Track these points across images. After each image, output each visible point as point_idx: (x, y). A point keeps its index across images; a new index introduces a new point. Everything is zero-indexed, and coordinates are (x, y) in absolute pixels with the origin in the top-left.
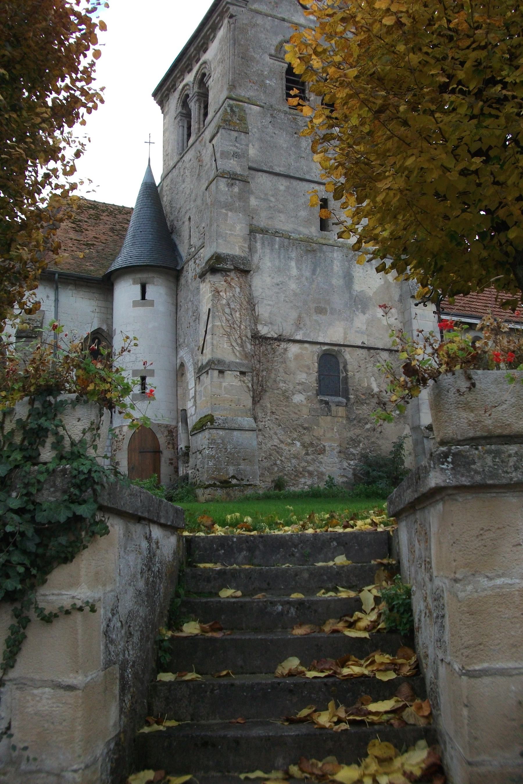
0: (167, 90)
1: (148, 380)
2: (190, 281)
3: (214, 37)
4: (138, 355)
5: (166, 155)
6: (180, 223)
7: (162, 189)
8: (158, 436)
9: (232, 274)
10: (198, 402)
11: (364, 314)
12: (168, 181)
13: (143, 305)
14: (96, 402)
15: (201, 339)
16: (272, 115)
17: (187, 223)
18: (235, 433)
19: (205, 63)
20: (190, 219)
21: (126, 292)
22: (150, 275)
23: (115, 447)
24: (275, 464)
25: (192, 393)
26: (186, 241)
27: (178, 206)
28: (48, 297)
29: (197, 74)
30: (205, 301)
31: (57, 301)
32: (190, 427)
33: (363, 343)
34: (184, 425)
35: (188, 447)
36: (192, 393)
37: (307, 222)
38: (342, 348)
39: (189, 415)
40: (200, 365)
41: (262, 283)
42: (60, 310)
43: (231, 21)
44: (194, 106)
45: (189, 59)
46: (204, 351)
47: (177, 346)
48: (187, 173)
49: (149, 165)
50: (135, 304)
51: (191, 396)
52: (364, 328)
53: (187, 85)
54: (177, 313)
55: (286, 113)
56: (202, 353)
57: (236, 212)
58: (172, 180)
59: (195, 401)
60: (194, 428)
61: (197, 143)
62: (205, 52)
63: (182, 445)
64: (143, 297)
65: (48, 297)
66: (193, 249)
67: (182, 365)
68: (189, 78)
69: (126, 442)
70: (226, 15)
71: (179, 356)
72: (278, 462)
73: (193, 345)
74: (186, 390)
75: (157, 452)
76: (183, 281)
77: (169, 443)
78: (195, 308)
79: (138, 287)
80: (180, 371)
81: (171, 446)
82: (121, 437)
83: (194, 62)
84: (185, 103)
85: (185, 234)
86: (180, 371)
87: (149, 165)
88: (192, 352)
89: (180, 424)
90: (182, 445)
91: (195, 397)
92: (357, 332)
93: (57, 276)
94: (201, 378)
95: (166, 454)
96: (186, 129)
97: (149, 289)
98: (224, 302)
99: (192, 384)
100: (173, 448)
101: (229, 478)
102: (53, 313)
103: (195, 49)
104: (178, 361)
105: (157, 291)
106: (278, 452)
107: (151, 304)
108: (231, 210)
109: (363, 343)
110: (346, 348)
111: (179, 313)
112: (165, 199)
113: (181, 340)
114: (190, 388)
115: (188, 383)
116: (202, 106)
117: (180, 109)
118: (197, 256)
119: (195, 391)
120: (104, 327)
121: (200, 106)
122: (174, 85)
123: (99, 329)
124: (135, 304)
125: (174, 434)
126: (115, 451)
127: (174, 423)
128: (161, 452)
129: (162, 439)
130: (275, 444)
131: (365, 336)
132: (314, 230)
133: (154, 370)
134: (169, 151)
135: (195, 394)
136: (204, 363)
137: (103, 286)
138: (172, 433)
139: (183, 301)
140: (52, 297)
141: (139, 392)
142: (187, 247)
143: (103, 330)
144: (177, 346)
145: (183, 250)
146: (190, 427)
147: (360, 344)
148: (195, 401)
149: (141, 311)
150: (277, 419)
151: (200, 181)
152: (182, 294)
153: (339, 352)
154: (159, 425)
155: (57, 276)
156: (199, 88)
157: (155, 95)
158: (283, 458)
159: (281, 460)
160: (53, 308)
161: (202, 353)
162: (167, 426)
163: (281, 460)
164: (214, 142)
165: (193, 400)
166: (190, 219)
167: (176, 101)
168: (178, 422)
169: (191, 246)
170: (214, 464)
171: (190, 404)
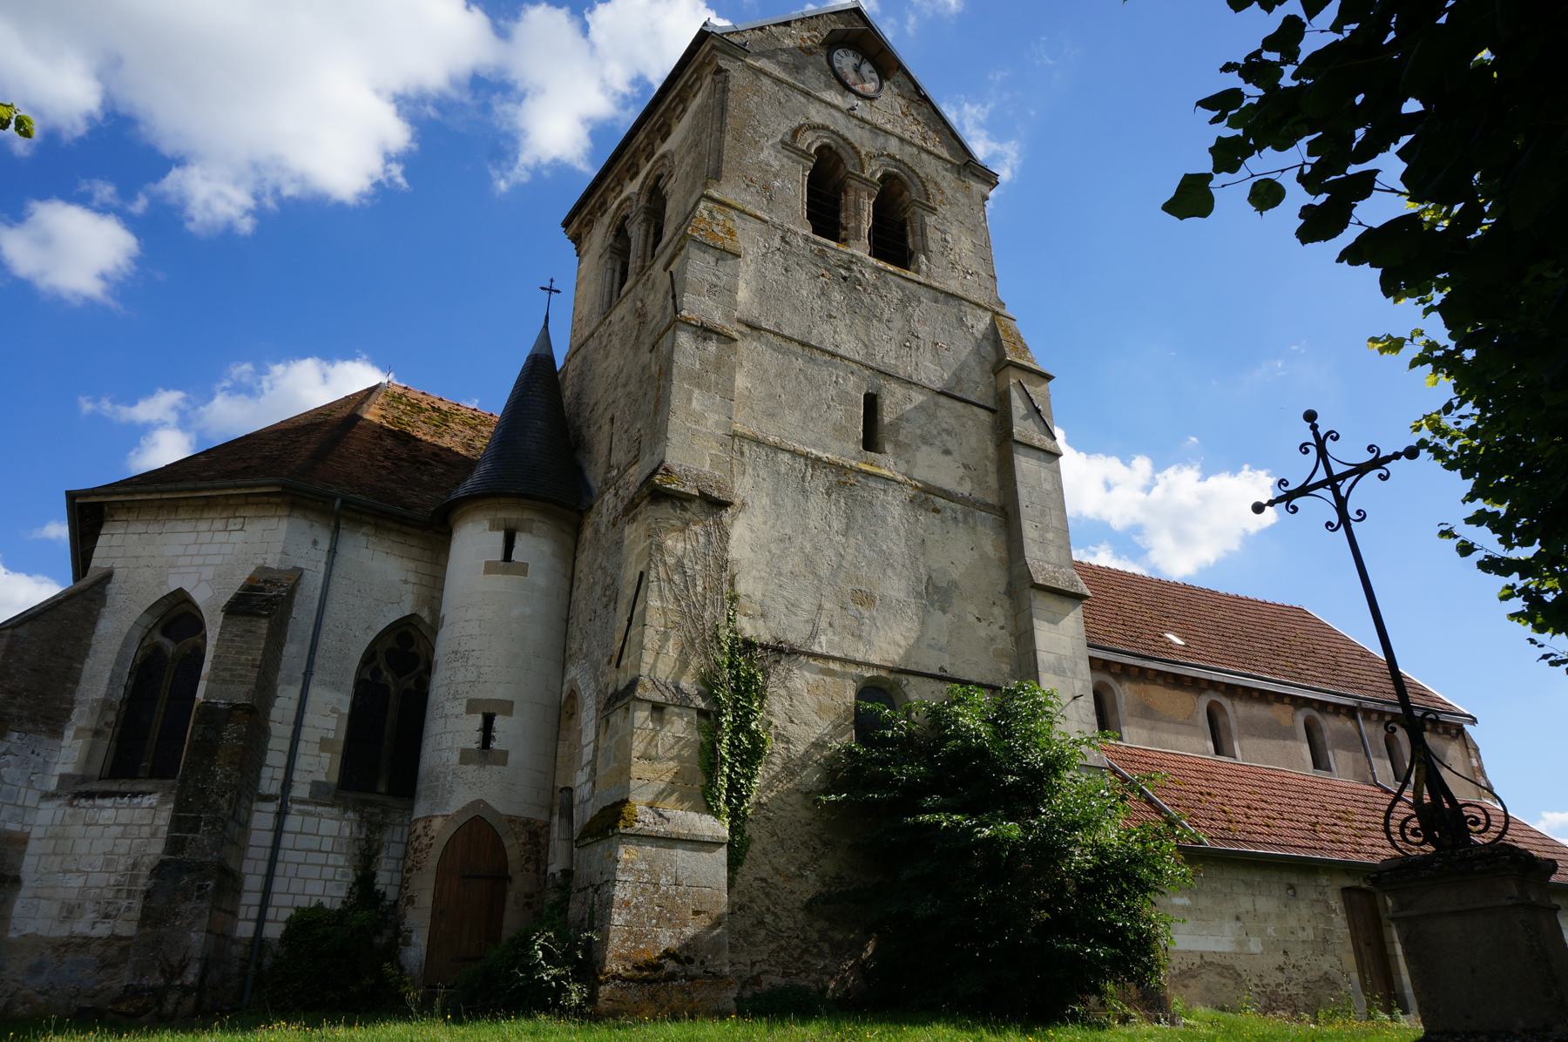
0: (590, 213)
1: (499, 722)
2: (603, 530)
3: (684, 110)
4: (484, 670)
5: (577, 321)
6: (594, 429)
7: (564, 376)
8: (507, 843)
9: (695, 507)
10: (601, 772)
11: (944, 611)
12: (577, 360)
13: (506, 572)
14: (1059, 778)
15: (619, 636)
16: (783, 238)
17: (606, 428)
18: (680, 854)
19: (664, 156)
20: (612, 419)
21: (475, 541)
22: (526, 515)
23: (410, 863)
24: (761, 923)
25: (587, 753)
26: (602, 460)
27: (592, 402)
28: (315, 543)
29: (646, 177)
30: (633, 558)
31: (333, 552)
32: (577, 827)
33: (941, 669)
34: (564, 821)
35: (567, 873)
36: (587, 753)
37: (840, 431)
38: (903, 677)
39: (576, 801)
40: (610, 691)
41: (745, 535)
42: (335, 570)
43: (718, 78)
44: (636, 232)
45: (633, 155)
46: (623, 663)
47: (563, 660)
48: (616, 341)
49: (546, 327)
50: (490, 568)
51: (584, 761)
52: (944, 640)
53: (628, 198)
54: (570, 593)
55: (807, 239)
56: (618, 666)
57: (709, 390)
58: (585, 358)
59: (594, 771)
60: (583, 836)
61: (640, 286)
62: (664, 140)
63: (555, 868)
64: (507, 556)
65: (315, 543)
66: (615, 473)
67: (573, 695)
68: (632, 187)
69: (435, 853)
70: (708, 69)
71: (568, 677)
72: (769, 919)
73: (598, 654)
74: (577, 745)
75: (501, 878)
76: (588, 533)
77: (528, 860)
78: (609, 580)
79: (499, 537)
80: (564, 711)
81: (531, 866)
82: (425, 841)
83: (642, 160)
84: (621, 232)
85: (601, 449)
86: (564, 711)
87: (546, 327)
88: (595, 667)
89: (556, 819)
90: (555, 868)
91: (593, 763)
92: (930, 646)
93: (338, 502)
94: (612, 719)
95: (519, 885)
96: (617, 275)
97: (522, 543)
98: (671, 561)
99: (589, 734)
100: (537, 870)
101: (659, 958)
102: (322, 575)
103: (647, 136)
104: (565, 687)
105: (533, 548)
106: (767, 895)
107: (523, 569)
108: (699, 386)
109: (941, 669)
110: (911, 678)
111: (575, 593)
112: (568, 393)
113: (575, 646)
114: (584, 742)
115: (581, 731)
116: (652, 231)
117: (610, 240)
118: (621, 482)
119: (596, 749)
120: (425, 614)
121: (648, 232)
122: (604, 203)
123: (413, 615)
124: (490, 568)
125: (542, 841)
126: (409, 870)
127: (543, 817)
128: (510, 879)
129: (514, 849)
130: (764, 875)
131: (947, 657)
132: (847, 451)
133: (512, 703)
134: (585, 311)
135: (595, 756)
136: (621, 688)
137: (431, 532)
138: (536, 836)
139: (586, 570)
140: (325, 545)
141: (475, 746)
142: (602, 471)
143: (422, 620)
144: (563, 660)
145: (595, 475)
146: (577, 827)
147: (936, 671)
148: (594, 771)
149: (500, 582)
150: (769, 819)
151: (638, 349)
152: (584, 558)
153: (898, 684)
154: (512, 820)
155: (338, 502)
156: (649, 200)
157: (566, 224)
158: (778, 910)
159: (774, 914)
160: (322, 567)
161: (618, 666)
162: (527, 822)
163: (774, 914)
164: (672, 268)
165: (587, 770)
166: (612, 419)
167: (603, 231)
168: (551, 815)
169: (610, 467)
170: (628, 923)
171: (580, 778)
